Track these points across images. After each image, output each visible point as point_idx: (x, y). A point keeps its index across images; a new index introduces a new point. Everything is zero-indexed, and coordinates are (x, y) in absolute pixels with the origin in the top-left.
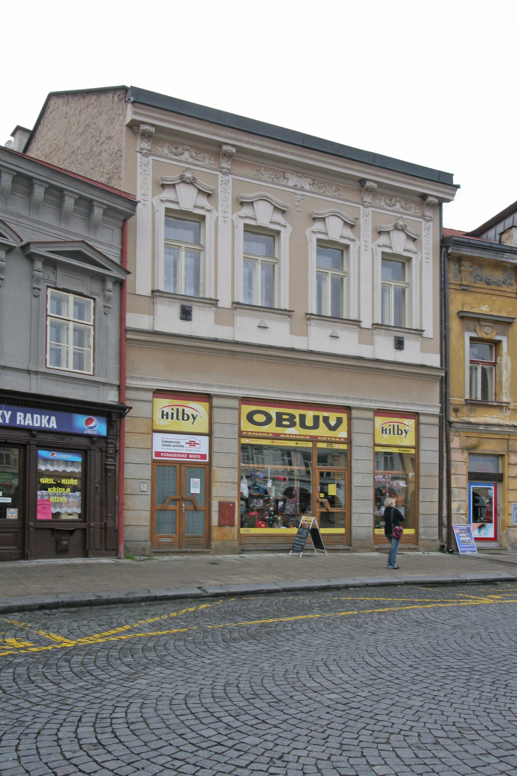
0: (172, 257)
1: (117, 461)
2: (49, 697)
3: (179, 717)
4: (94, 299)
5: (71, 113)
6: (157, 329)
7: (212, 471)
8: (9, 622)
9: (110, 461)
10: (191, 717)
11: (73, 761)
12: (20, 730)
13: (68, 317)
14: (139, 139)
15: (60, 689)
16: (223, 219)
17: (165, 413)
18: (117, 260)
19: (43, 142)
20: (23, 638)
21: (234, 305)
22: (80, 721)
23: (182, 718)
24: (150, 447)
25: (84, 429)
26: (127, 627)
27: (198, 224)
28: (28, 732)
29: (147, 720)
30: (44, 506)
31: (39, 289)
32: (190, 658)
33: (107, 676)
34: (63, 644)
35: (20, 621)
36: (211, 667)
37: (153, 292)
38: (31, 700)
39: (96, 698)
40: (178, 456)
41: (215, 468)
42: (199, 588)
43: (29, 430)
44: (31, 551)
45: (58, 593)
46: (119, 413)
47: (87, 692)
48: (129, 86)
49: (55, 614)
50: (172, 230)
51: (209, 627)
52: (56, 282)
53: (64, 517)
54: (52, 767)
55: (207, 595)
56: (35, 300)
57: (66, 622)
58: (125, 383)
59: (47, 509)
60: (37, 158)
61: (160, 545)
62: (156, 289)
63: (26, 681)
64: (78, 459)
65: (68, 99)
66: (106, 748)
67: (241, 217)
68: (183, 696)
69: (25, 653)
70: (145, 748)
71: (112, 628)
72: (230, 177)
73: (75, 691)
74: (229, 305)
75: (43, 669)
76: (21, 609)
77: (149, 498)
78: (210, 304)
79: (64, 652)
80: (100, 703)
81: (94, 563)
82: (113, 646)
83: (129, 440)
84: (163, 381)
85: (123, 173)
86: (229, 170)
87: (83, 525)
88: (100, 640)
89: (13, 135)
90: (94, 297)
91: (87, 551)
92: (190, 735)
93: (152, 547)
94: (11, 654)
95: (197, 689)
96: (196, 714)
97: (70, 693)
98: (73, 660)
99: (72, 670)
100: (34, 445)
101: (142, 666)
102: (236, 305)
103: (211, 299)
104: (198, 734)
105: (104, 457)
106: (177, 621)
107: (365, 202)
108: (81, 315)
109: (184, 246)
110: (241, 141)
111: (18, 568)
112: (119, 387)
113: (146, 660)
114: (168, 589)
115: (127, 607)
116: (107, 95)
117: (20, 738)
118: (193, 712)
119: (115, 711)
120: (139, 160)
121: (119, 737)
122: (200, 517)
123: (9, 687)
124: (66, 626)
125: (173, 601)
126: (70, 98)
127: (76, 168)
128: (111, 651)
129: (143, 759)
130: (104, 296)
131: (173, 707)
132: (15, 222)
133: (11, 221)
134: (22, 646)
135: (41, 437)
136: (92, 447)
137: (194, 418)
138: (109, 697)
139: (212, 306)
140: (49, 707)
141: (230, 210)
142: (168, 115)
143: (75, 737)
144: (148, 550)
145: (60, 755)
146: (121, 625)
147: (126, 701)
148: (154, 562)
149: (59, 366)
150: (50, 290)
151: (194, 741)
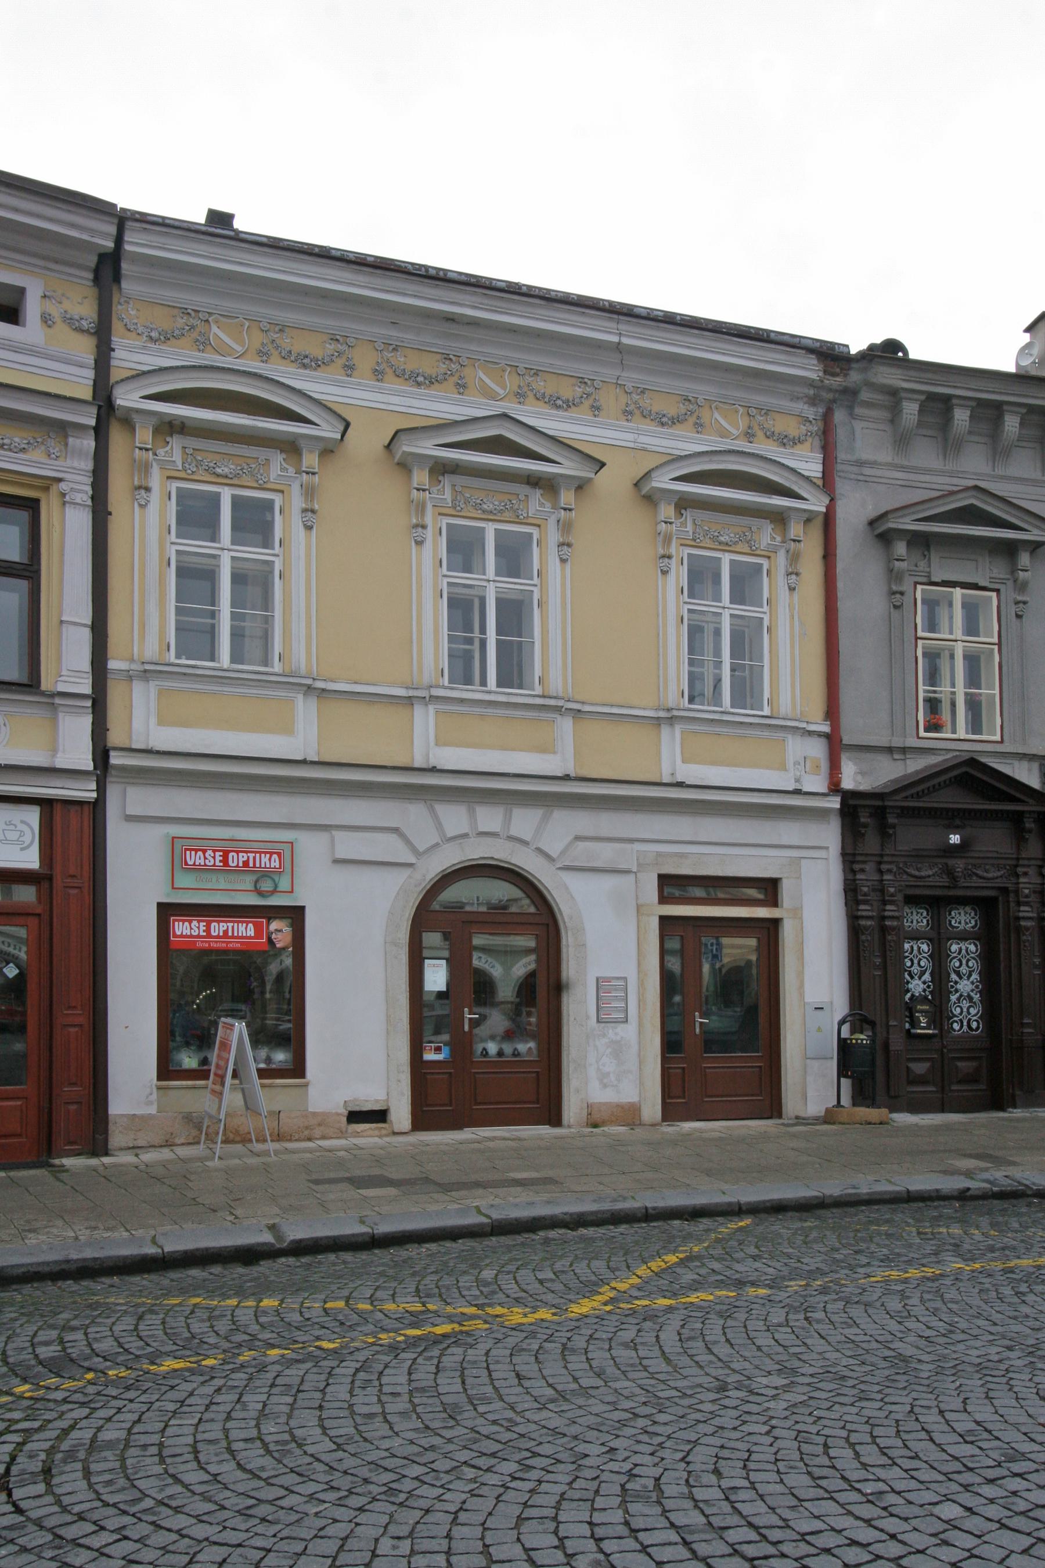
4: (998, 591)
13: (951, 633)
31: (902, 593)
52: (929, 572)
56: (895, 614)
105: (1012, 905)
108: (972, 628)
130: (1015, 581)
150: (919, 587)
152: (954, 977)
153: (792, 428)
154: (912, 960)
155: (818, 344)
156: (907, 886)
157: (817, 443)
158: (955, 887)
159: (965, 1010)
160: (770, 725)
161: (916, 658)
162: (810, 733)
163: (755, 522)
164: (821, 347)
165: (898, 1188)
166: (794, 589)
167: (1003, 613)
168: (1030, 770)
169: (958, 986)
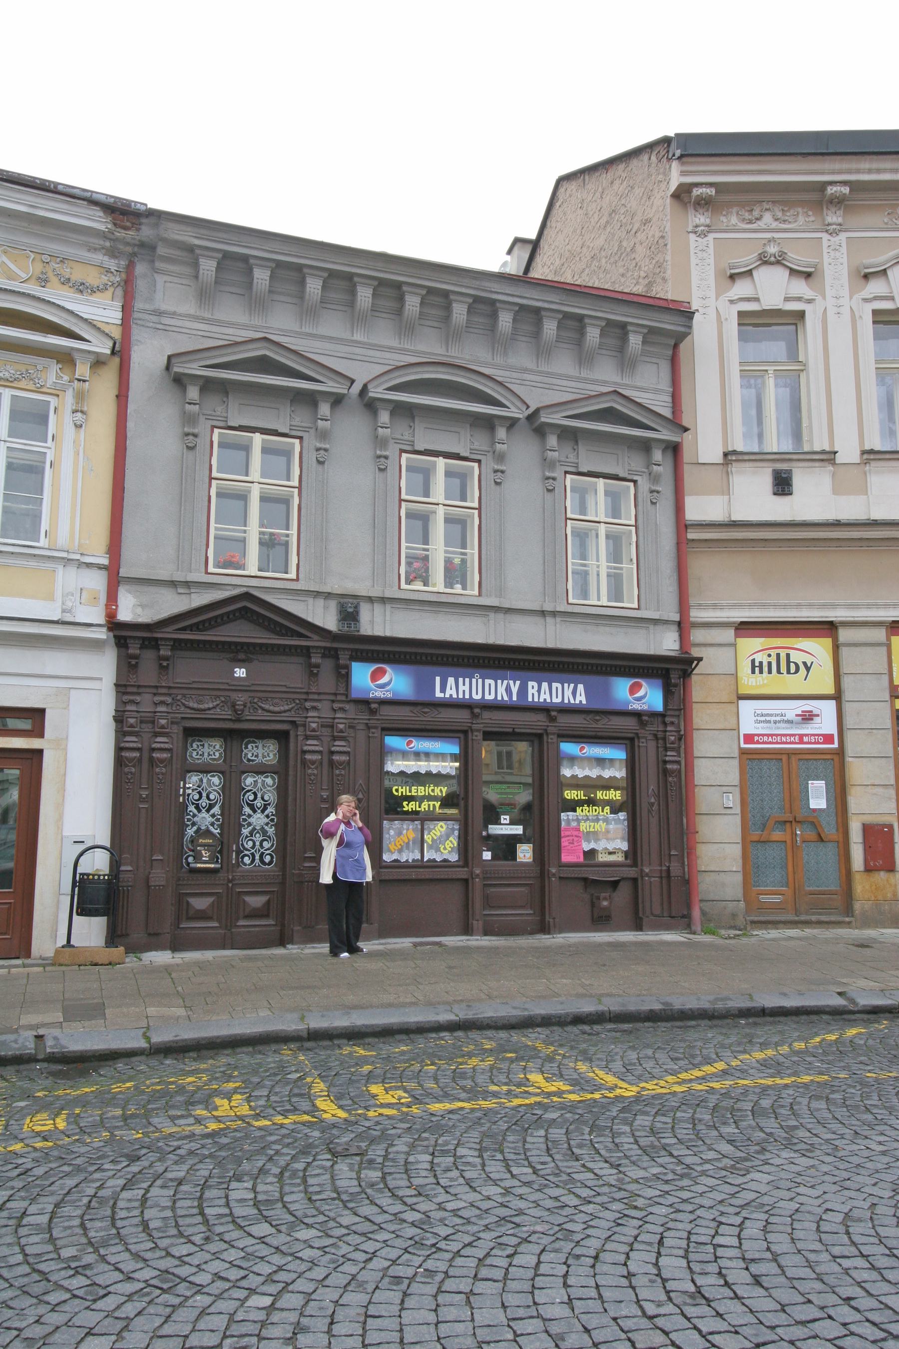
0: (753, 391)
1: (683, 755)
2: (605, 1189)
3: (838, 1260)
4: (635, 482)
5: (589, 198)
6: (737, 517)
7: (847, 765)
8: (530, 1043)
9: (671, 755)
10: (860, 1262)
11: (659, 1322)
12: (567, 1246)
14: (691, 211)
15: (621, 1176)
16: (836, 310)
17: (757, 664)
18: (667, 412)
19: (551, 252)
20: (554, 1074)
21: (865, 456)
22: (661, 1242)
23: (846, 1263)
24: (735, 727)
25: (628, 703)
26: (721, 1066)
27: (793, 327)
28: (579, 1253)
29: (779, 1258)
30: (571, 838)
31: (554, 479)
32: (842, 1137)
33: (696, 1160)
34: (618, 1092)
35: (548, 1042)
36: (886, 1159)
37: (726, 455)
38: (578, 1191)
39: (684, 1201)
40: (784, 739)
41: (850, 759)
42: (840, 994)
43: (545, 710)
44: (554, 918)
45: (602, 995)
46: (682, 670)
47: (666, 1188)
48: (671, 134)
49: (598, 1034)
50: (750, 346)
51: (868, 1075)
52: (577, 463)
53: (602, 858)
54: (626, 1329)
55: (856, 1009)
56: (548, 496)
57: (617, 1050)
58: (689, 616)
59: (576, 844)
60: (543, 278)
61: (763, 908)
62: (730, 449)
63: (567, 1155)
64: (619, 754)
65: (584, 180)
66: (712, 1304)
67: (866, 300)
68: (839, 1217)
69: (560, 1103)
70: (782, 1318)
71: (695, 1066)
72: (843, 236)
73: (645, 1182)
74: (855, 458)
75: (590, 1134)
76: (546, 1022)
77: (738, 819)
78: (822, 460)
79: (621, 1105)
80: (690, 1212)
81: (652, 941)
82: (701, 1103)
83: (701, 717)
84: (751, 606)
85: (669, 272)
86: (840, 225)
87: (632, 872)
88: (678, 1089)
89: (509, 252)
90: (635, 478)
91: (641, 919)
92: (865, 1303)
93: (748, 911)
94: (539, 1103)
95: (866, 1205)
96: (870, 1259)
97: (639, 1186)
98: (636, 1123)
99: (636, 1142)
100: (554, 734)
101: (756, 1144)
102: (870, 455)
103: (823, 452)
104: (881, 1302)
105: (661, 749)
106: (808, 1059)
107: (829, 225)
108: (615, 511)
109: (771, 369)
110: (858, 171)
111: (537, 948)
112: (679, 624)
113: (762, 1135)
114: (785, 994)
115: (715, 1026)
116: (641, 157)
117: (569, 1262)
118: (865, 1253)
119: (720, 1231)
120: (692, 245)
121: (733, 1287)
122: (829, 853)
123: (542, 1163)
124: (618, 1057)
125: (794, 1018)
126: (587, 177)
127: (599, 279)
128: (698, 1110)
129: (782, 1339)
131: (823, 1236)
132: (518, 382)
133: (513, 381)
134: (554, 1089)
135: (564, 721)
136: (642, 732)
137: (808, 669)
138: (706, 1202)
139: (826, 464)
140: (607, 1209)
141: (846, 292)
142: (735, 162)
143: (657, 1275)
144: (741, 917)
145: (635, 1306)
146: (709, 1061)
147: (737, 1214)
148: (753, 940)
149: (586, 598)
151: (875, 1317)
152: (247, 810)
153: (93, 278)
154: (255, 794)
155: (112, 200)
156: (183, 718)
157: (119, 292)
158: (238, 720)
159: (258, 843)
160: (35, 555)
161: (210, 497)
162: (89, 565)
163: (41, 361)
164: (115, 202)
165: (894, 1002)
166: (81, 426)
167: (304, 459)
168: (326, 608)
169: (251, 820)
